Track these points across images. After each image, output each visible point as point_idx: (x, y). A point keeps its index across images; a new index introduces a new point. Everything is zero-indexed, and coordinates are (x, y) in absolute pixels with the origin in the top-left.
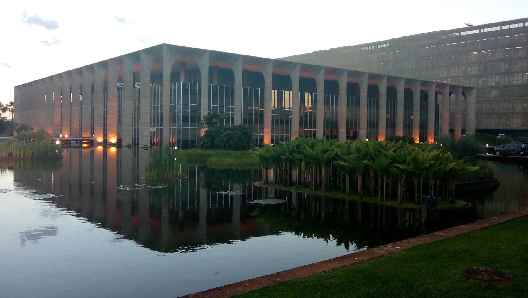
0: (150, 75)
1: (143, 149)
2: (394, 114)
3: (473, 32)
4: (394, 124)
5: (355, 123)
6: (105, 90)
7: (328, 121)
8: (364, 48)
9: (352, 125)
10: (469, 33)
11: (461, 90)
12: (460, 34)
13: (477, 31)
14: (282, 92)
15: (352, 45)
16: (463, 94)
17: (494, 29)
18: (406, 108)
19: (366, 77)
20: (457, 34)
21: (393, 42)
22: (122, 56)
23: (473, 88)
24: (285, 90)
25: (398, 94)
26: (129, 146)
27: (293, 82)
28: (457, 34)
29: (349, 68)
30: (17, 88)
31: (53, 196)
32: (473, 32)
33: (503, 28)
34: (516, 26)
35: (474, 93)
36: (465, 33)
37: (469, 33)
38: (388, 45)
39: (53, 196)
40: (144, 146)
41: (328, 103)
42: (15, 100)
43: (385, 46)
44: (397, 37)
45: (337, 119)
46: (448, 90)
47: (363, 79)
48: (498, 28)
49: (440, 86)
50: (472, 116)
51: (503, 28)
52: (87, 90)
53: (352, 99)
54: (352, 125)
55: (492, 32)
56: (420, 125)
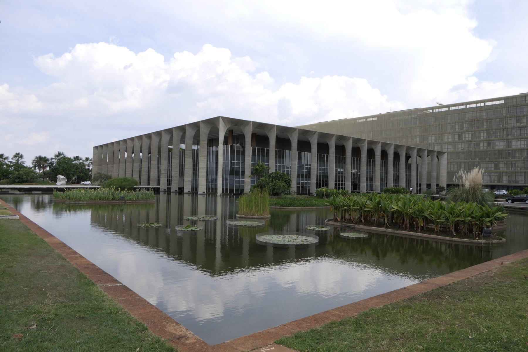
0: (207, 140)
1: (202, 196)
2: (373, 170)
3: (443, 110)
4: (372, 178)
6: (159, 151)
8: (358, 121)
10: (440, 110)
11: (436, 154)
12: (433, 111)
15: (348, 118)
16: (437, 157)
17: (460, 107)
19: (366, 143)
20: (431, 111)
21: (380, 116)
22: (185, 125)
24: (305, 152)
25: (389, 156)
26: (188, 193)
27: (312, 146)
28: (431, 111)
30: (96, 148)
32: (443, 110)
33: (468, 106)
34: (478, 105)
35: (445, 156)
36: (437, 110)
37: (440, 110)
38: (376, 119)
41: (320, 161)
42: (93, 157)
43: (362, 120)
44: (383, 112)
45: (373, 176)
46: (426, 153)
48: (464, 107)
50: (444, 174)
51: (468, 106)
52: (145, 149)
55: (473, 108)
56: (367, 178)
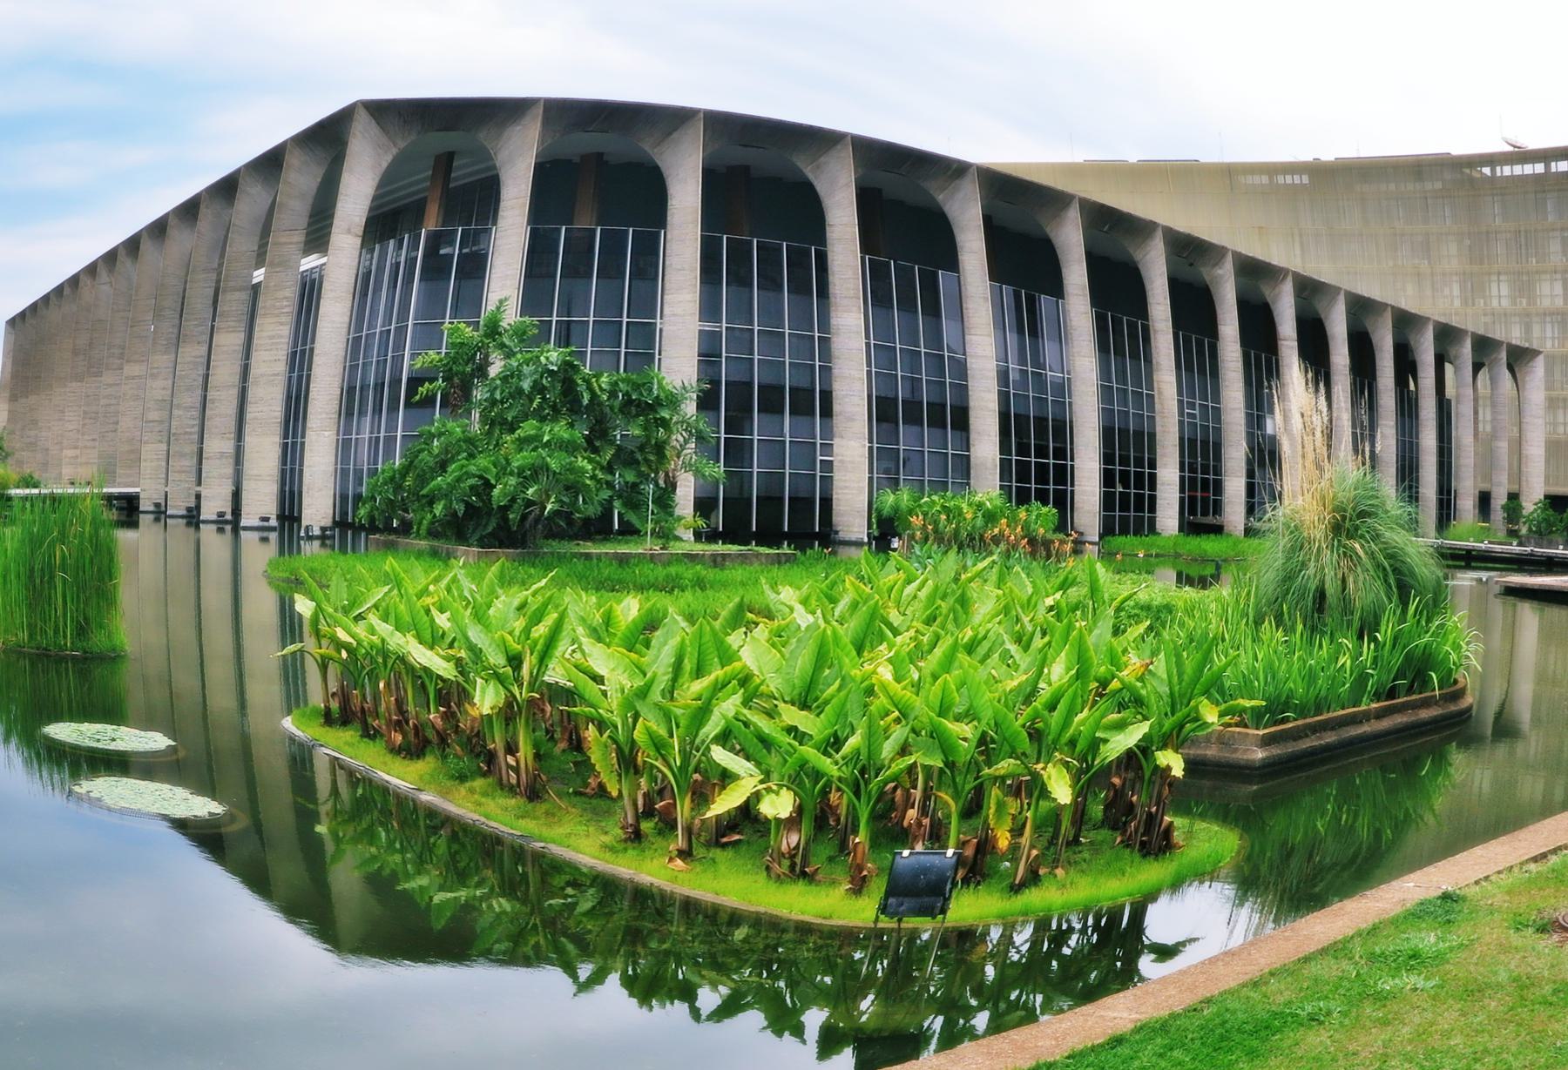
3: (1528, 169)
5: (1139, 434)
7: (1022, 419)
9: (1124, 446)
10: (1518, 170)
13: (1540, 168)
14: (1032, 303)
18: (1403, 415)
23: (1536, 353)
26: (220, 522)
29: (1083, 195)
31: (202, 807)
32: (1528, 169)
37: (1518, 170)
39: (202, 807)
40: (214, 517)
47: (1220, 272)
49: (1447, 336)
53: (1258, 359)
54: (1124, 446)
